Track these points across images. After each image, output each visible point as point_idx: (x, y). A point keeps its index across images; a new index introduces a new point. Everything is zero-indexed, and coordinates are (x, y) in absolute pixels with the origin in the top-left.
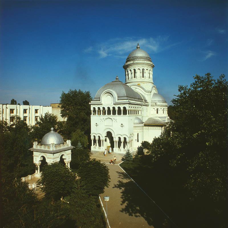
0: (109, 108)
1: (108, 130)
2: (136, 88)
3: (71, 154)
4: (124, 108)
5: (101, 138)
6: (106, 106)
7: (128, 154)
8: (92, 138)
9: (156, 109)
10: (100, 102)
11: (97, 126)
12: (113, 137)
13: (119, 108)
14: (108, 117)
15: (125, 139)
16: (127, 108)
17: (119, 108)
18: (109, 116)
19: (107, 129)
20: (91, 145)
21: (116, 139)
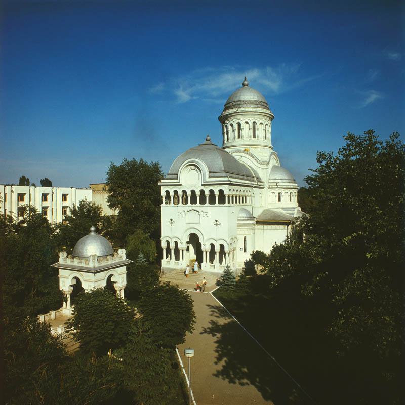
2: (242, 157)
3: (127, 273)
4: (221, 192)
5: (180, 246)
8: (164, 245)
9: (277, 194)
10: (178, 181)
11: (172, 223)
12: (200, 244)
13: (212, 192)
14: (191, 208)
16: (226, 192)
17: (212, 192)
18: (194, 207)
19: (191, 228)
20: (162, 258)
21: (206, 247)
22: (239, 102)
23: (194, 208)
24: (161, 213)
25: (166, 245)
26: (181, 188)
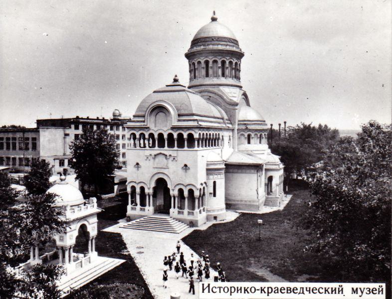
0: (161, 135)
1: (160, 132)
2: (210, 97)
3: (98, 223)
4: (190, 136)
5: (147, 191)
6: (156, 132)
7: (117, 157)
8: (129, 190)
9: (246, 136)
10: (145, 123)
11: (138, 168)
12: (169, 189)
13: (180, 136)
14: (159, 152)
15: (142, 189)
16: (196, 136)
17: (180, 136)
18: (162, 151)
19: (159, 173)
20: (128, 204)
21: (174, 192)
22: (208, 39)
23: (162, 152)
24: (348, 282)
25: (276, 275)
26: (148, 131)
